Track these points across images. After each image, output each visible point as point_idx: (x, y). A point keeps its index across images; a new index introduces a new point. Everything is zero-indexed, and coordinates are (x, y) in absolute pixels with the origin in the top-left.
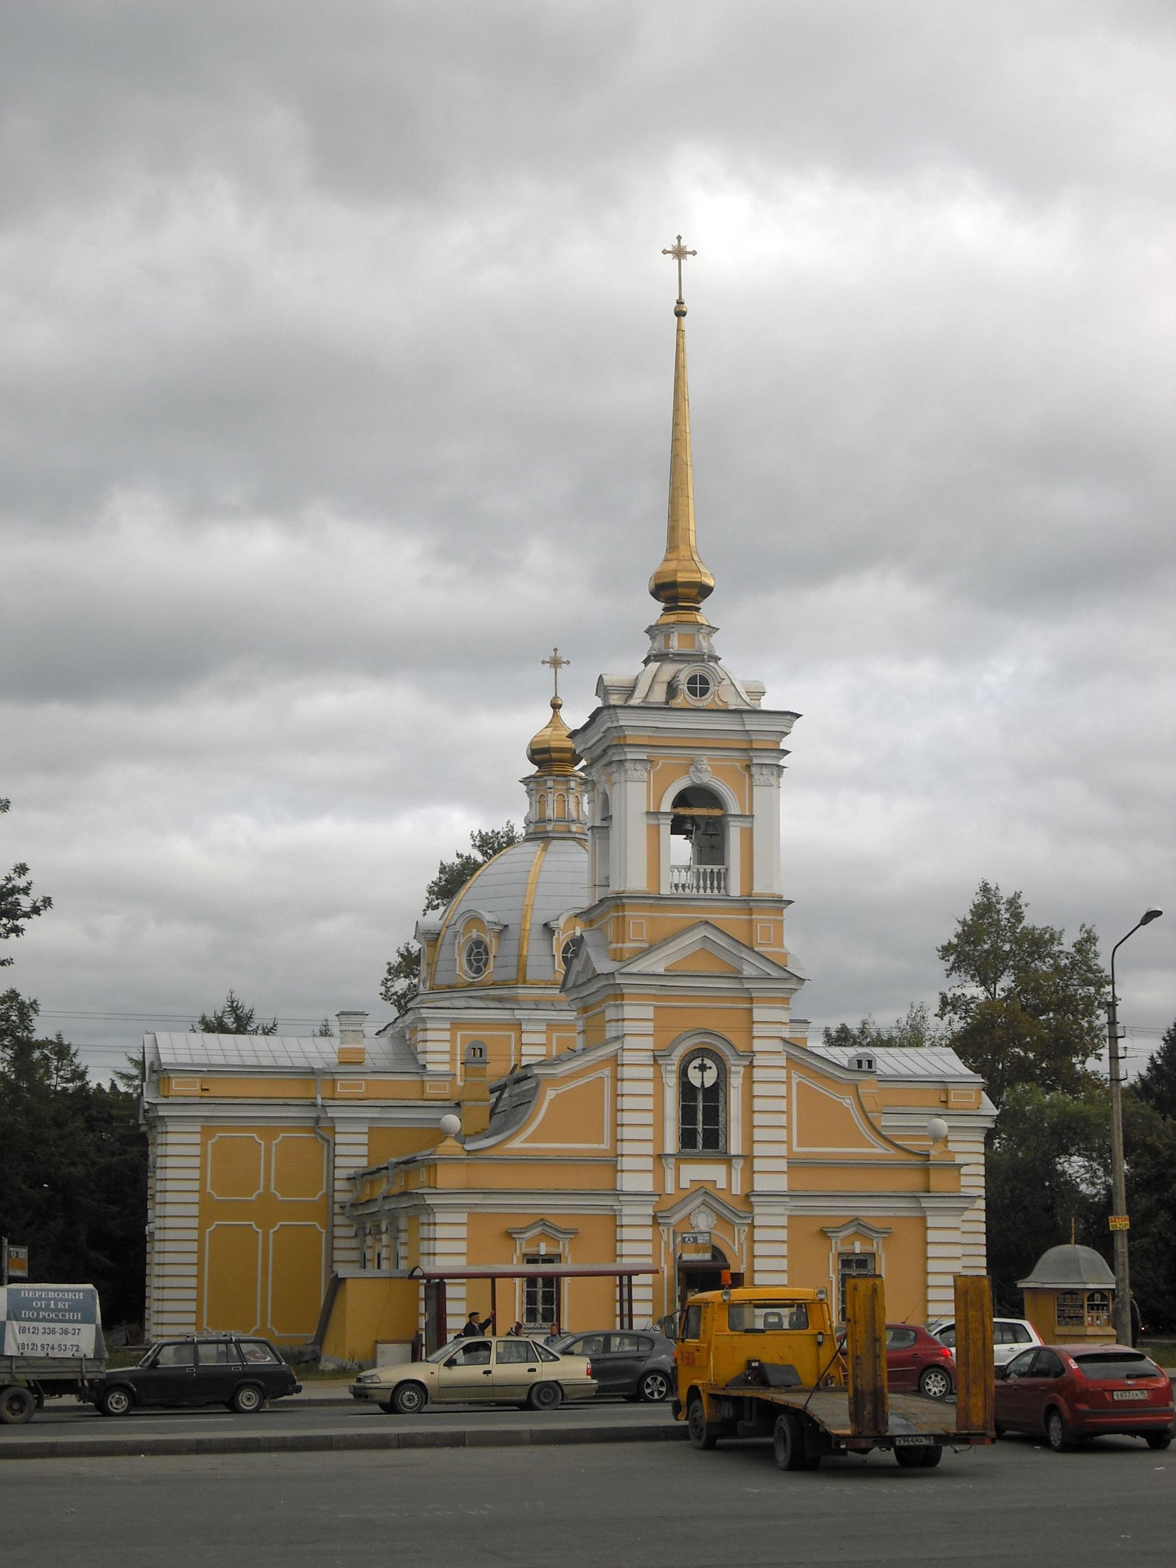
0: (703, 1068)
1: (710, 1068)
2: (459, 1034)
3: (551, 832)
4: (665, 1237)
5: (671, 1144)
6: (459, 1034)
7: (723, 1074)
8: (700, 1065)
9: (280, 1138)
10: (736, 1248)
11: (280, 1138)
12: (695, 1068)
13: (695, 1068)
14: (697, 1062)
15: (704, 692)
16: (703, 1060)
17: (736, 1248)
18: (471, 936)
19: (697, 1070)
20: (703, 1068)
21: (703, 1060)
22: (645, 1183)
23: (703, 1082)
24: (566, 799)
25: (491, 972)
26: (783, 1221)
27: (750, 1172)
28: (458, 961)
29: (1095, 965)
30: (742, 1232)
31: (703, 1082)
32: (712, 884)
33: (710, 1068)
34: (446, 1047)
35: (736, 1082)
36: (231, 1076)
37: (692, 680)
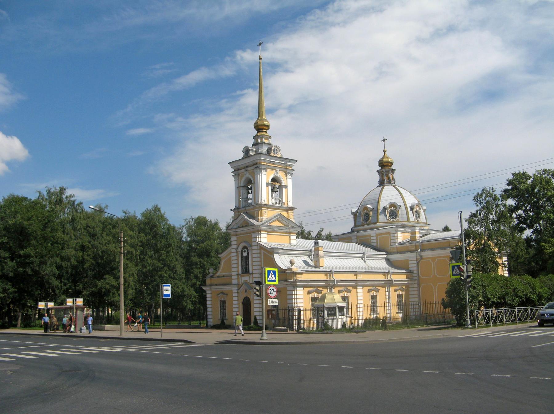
0: (245, 251)
2: (378, 237)
14: (244, 250)
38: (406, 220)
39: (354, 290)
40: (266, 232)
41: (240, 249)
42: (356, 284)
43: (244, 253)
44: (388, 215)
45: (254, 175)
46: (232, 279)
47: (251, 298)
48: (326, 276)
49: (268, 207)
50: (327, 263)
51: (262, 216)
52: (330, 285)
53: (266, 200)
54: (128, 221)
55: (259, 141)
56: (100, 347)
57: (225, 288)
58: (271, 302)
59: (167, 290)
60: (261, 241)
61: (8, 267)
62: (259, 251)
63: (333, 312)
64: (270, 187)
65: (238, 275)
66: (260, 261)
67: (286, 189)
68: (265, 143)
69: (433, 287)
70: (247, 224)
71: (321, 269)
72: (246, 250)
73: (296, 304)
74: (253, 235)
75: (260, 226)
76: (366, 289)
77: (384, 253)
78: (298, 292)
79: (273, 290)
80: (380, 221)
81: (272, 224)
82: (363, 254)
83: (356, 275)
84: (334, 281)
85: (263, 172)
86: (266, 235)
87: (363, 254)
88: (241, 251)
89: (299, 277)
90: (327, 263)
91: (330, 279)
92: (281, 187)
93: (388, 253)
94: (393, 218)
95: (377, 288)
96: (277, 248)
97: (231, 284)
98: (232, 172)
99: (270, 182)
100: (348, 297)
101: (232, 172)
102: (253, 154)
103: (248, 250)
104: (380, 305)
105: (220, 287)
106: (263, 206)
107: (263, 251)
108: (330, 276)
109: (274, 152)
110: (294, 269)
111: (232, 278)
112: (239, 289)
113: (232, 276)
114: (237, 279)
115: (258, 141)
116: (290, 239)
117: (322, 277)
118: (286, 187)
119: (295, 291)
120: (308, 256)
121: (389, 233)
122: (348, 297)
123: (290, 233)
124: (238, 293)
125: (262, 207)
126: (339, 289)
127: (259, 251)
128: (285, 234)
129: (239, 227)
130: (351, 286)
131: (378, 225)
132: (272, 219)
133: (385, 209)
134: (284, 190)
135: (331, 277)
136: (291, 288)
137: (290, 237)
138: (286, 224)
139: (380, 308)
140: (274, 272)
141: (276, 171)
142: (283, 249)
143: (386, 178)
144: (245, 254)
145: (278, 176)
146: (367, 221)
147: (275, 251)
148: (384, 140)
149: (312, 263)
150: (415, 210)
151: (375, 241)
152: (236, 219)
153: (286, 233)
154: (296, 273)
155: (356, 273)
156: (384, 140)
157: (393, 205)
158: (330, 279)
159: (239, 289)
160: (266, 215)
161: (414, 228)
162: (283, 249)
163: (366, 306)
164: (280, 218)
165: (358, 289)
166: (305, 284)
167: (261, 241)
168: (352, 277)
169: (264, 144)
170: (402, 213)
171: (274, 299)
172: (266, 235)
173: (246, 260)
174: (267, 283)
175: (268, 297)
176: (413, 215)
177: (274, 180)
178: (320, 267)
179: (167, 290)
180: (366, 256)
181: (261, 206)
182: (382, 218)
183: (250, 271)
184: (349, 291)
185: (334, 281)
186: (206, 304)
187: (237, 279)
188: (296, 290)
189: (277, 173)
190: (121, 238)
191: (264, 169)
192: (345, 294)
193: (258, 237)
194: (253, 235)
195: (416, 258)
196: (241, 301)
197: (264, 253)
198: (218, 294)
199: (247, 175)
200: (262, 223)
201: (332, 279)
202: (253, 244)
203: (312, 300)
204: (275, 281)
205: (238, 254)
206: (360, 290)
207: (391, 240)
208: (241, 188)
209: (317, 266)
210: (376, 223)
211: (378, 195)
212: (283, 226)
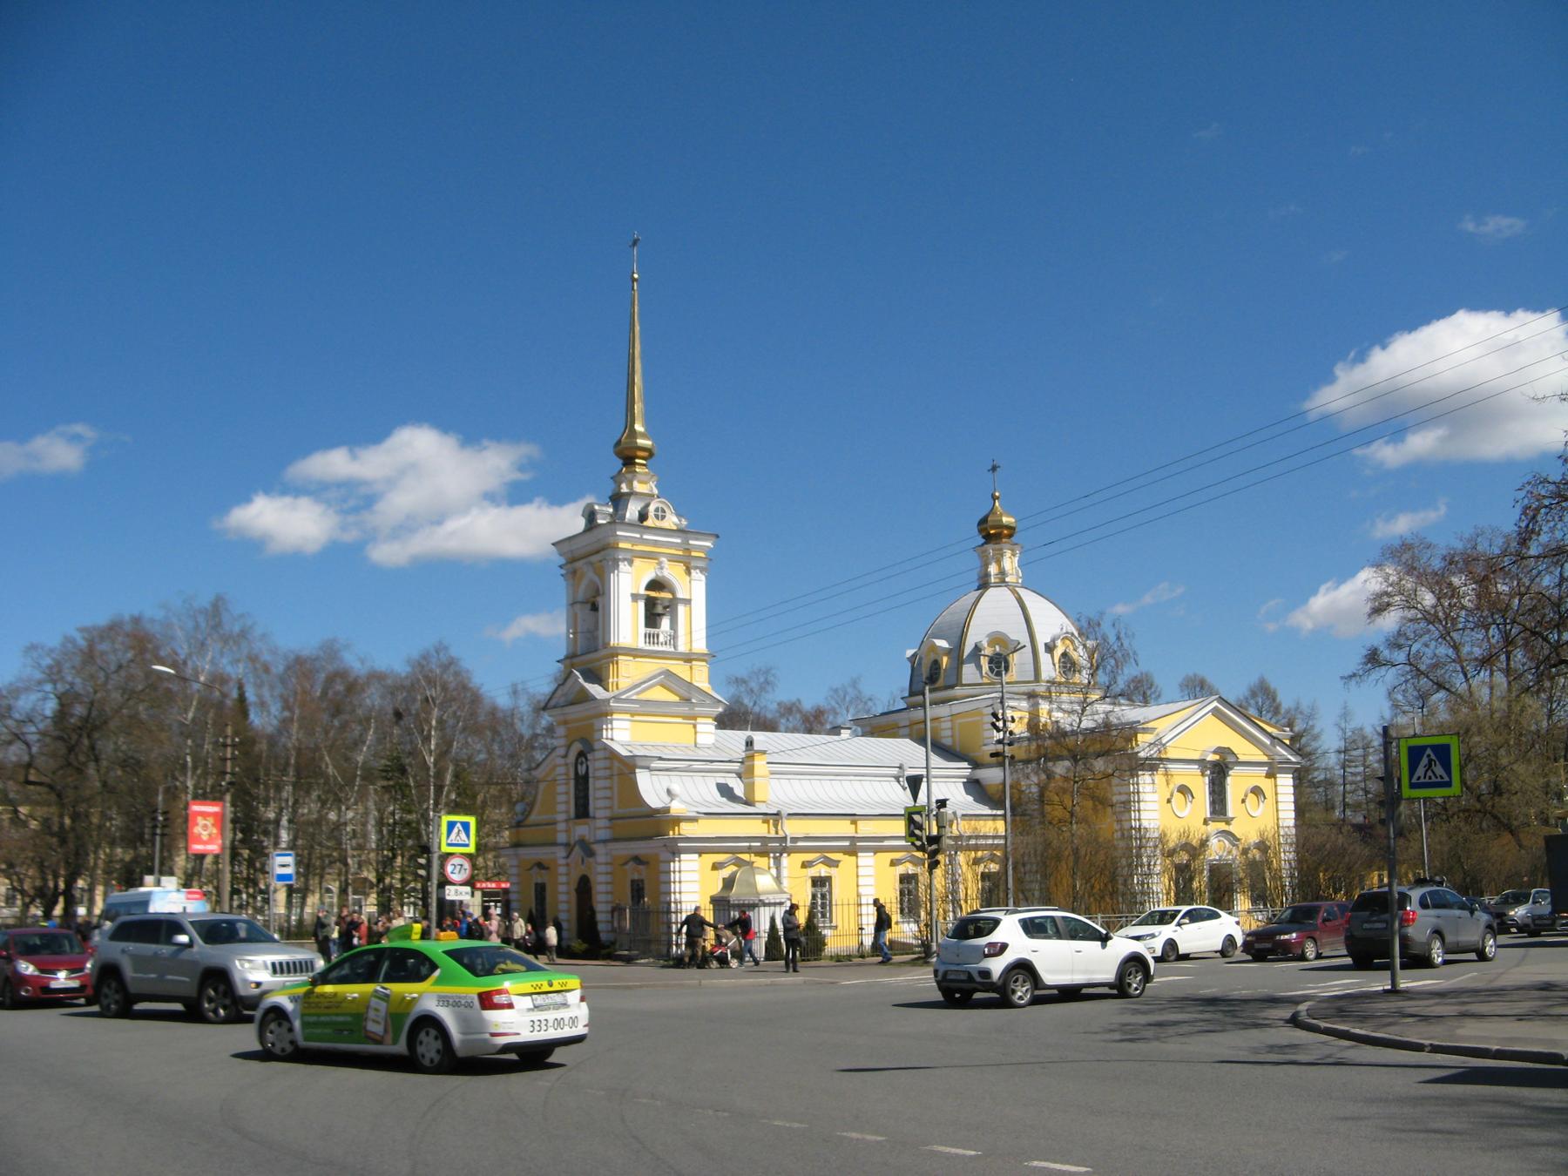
0: (582, 763)
14: (580, 761)
38: (1032, 679)
39: (846, 861)
40: (627, 716)
42: (853, 847)
43: (579, 767)
44: (985, 667)
46: (556, 831)
47: (592, 878)
48: (766, 825)
49: (634, 653)
50: (772, 791)
52: (775, 848)
54: (376, 677)
55: (624, 488)
56: (1525, 1069)
57: (541, 854)
58: (453, 892)
59: (284, 866)
60: (612, 739)
61: (1252, 702)
62: (607, 763)
63: (234, 910)
64: (641, 604)
65: (567, 821)
66: (611, 788)
67: (688, 608)
68: (637, 494)
70: (586, 697)
71: (761, 808)
73: (678, 895)
74: (595, 721)
75: (608, 701)
76: (711, 858)
77: (965, 765)
78: (684, 866)
79: (461, 865)
80: (964, 682)
81: (643, 696)
82: (900, 767)
83: (854, 823)
84: (785, 838)
85: (623, 566)
86: (628, 723)
87: (900, 767)
89: (687, 829)
90: (772, 791)
91: (777, 833)
92: (671, 607)
93: (976, 765)
95: (740, 856)
97: (554, 844)
98: (561, 567)
99: (642, 591)
100: (829, 879)
101: (561, 567)
102: (604, 522)
104: (839, 902)
105: (633, 845)
106: (619, 651)
108: (776, 826)
109: (657, 517)
110: (677, 808)
112: (568, 857)
114: (566, 831)
115: (620, 488)
116: (696, 733)
117: (757, 828)
118: (688, 602)
119: (677, 863)
120: (737, 774)
122: (829, 879)
123: (695, 718)
124: (568, 865)
125: (617, 655)
126: (715, 860)
127: (607, 763)
128: (680, 720)
129: (572, 704)
130: (749, 850)
131: (958, 691)
132: (644, 682)
133: (977, 649)
134: (681, 609)
135: (779, 827)
136: (667, 856)
137: (695, 726)
138: (686, 695)
139: (839, 908)
140: (466, 826)
141: (660, 563)
142: (660, 759)
143: (993, 569)
144: (581, 770)
145: (664, 577)
147: (639, 762)
148: (994, 469)
149: (739, 789)
150: (1058, 652)
151: (948, 733)
152: (563, 684)
153: (685, 718)
154: (677, 820)
155: (853, 817)
156: (994, 469)
157: (997, 639)
158: (777, 833)
159: (568, 857)
160: (626, 673)
162: (660, 759)
163: (846, 902)
164: (669, 679)
165: (859, 859)
166: (702, 847)
167: (612, 739)
168: (843, 828)
169: (632, 497)
170: (1019, 664)
171: (461, 885)
172: (627, 724)
173: (582, 782)
174: (445, 849)
175: (444, 882)
176: (1054, 665)
177: (655, 585)
178: (757, 804)
179: (284, 866)
182: (969, 672)
183: (591, 814)
185: (785, 838)
187: (566, 831)
188: (680, 861)
189: (662, 568)
190: (226, 737)
191: (625, 559)
192: (822, 870)
193: (607, 729)
196: (574, 885)
198: (626, 863)
200: (616, 692)
201: (781, 834)
202: (597, 746)
203: (901, 881)
204: (467, 845)
206: (866, 859)
208: (578, 606)
209: (749, 802)
210: (952, 687)
211: (966, 614)
212: (676, 699)
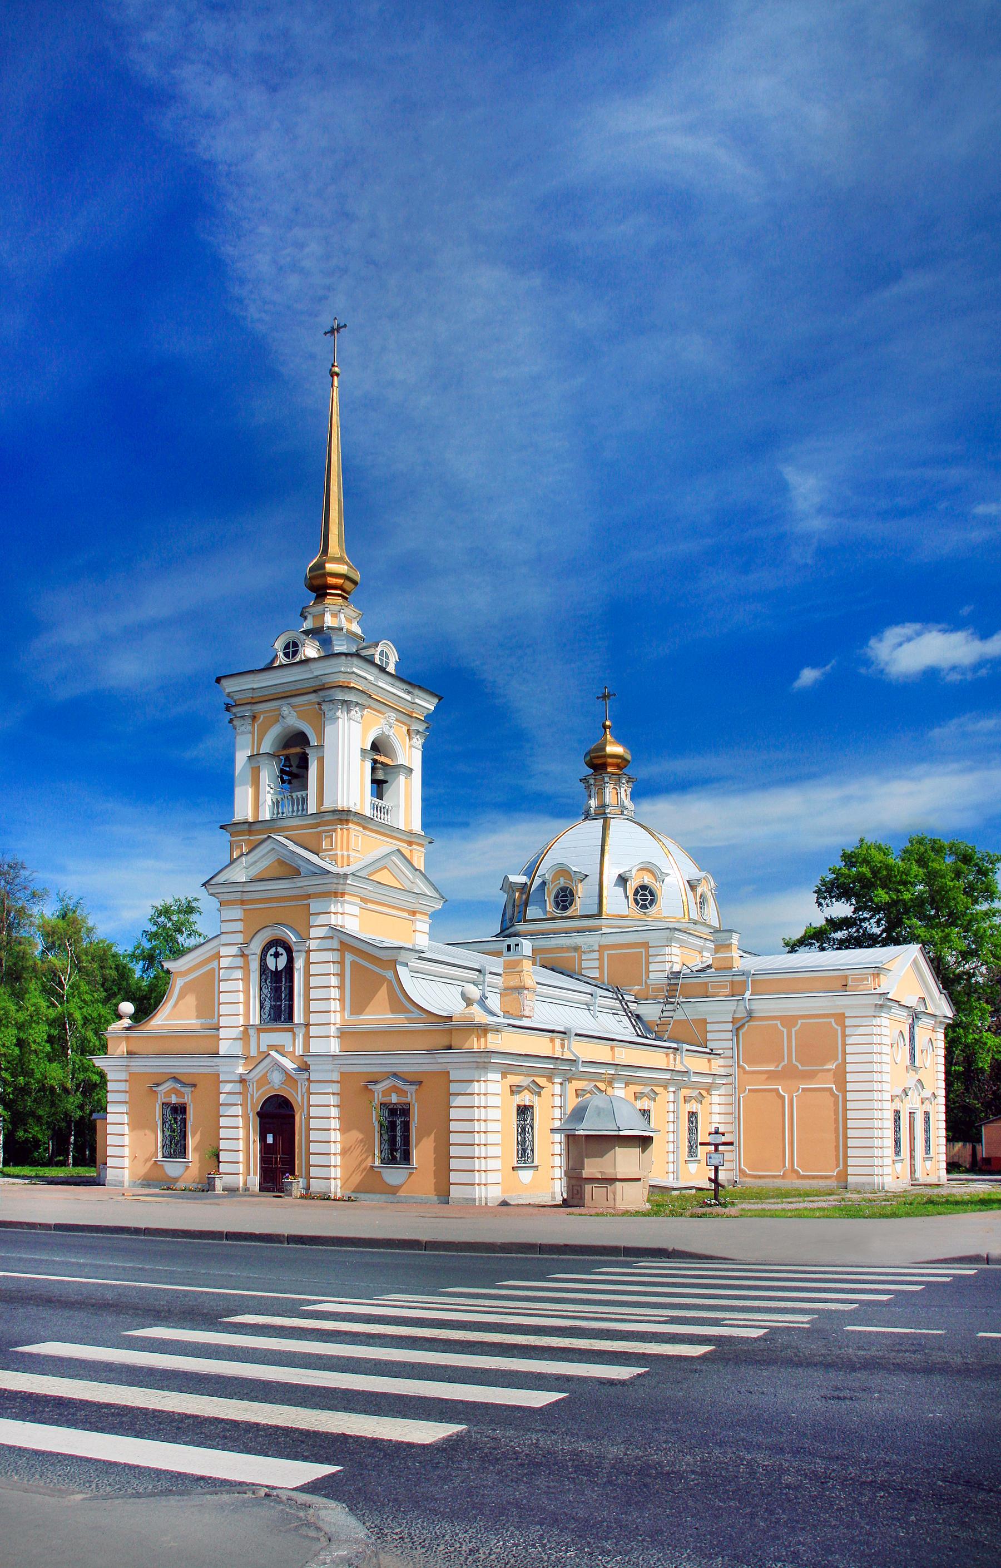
0: (277, 955)
1: (282, 954)
2: (606, 953)
3: (609, 813)
4: (251, 1090)
5: (255, 1019)
6: (606, 953)
7: (290, 960)
8: (275, 953)
9: (782, 1028)
10: (299, 1099)
11: (782, 1028)
12: (271, 955)
13: (271, 955)
14: (272, 951)
15: (295, 653)
16: (276, 949)
17: (299, 1099)
18: (559, 883)
19: (273, 957)
20: (277, 955)
21: (276, 949)
22: (238, 1049)
23: (276, 967)
24: (619, 791)
25: (578, 907)
26: (336, 1076)
27: (307, 1037)
28: (548, 901)
29: (876, 896)
30: (303, 1085)
31: (276, 967)
32: (298, 808)
33: (282, 954)
34: (596, 964)
35: (299, 964)
36: (302, 979)
37: (287, 647)
41: (256, 947)
45: (320, 718)
51: (348, 850)
53: (358, 804)
69: (784, 1097)
72: (281, 950)
74: (315, 906)
88: (259, 952)
94: (644, 907)
96: (400, 948)
103: (289, 951)
107: (349, 957)
108: (563, 1046)
111: (219, 1036)
113: (218, 1029)
121: (646, 945)
146: (565, 908)
147: (403, 956)
150: (699, 890)
161: (728, 934)
172: (356, 910)
180: (598, 1001)
181: (345, 817)
184: (653, 1096)
186: (946, 1113)
194: (315, 906)
195: (733, 1018)
197: (353, 963)
199: (293, 721)
205: (247, 963)
207: (648, 963)
